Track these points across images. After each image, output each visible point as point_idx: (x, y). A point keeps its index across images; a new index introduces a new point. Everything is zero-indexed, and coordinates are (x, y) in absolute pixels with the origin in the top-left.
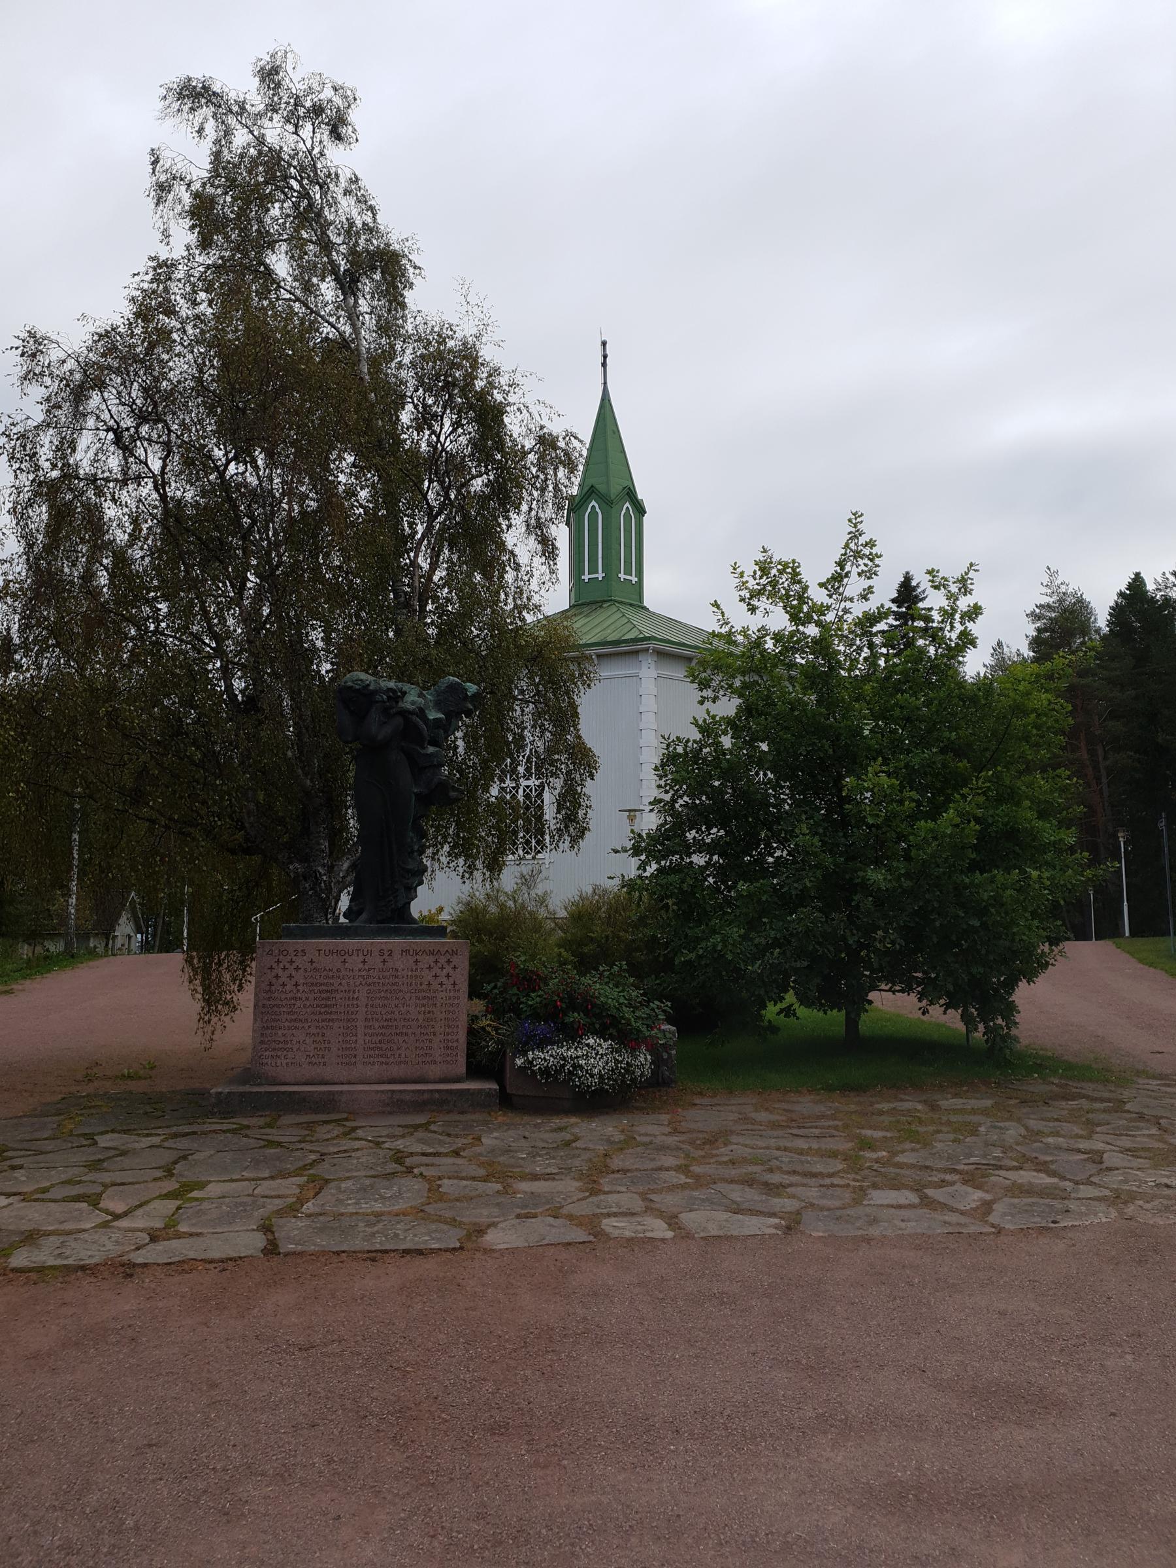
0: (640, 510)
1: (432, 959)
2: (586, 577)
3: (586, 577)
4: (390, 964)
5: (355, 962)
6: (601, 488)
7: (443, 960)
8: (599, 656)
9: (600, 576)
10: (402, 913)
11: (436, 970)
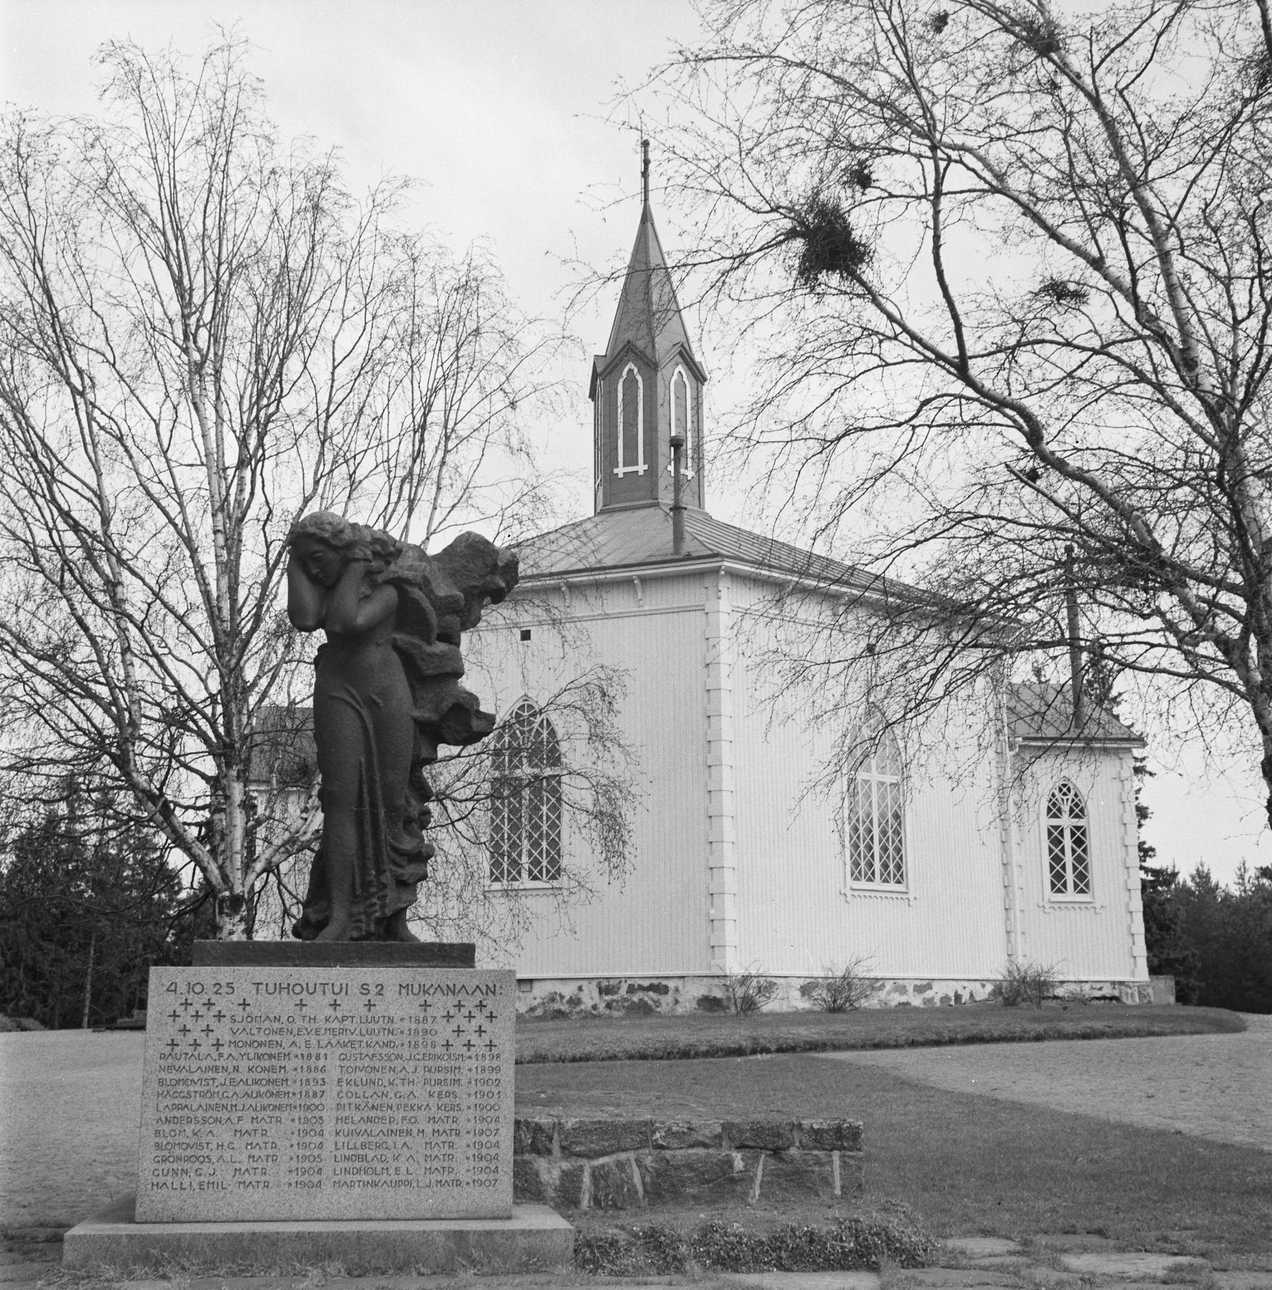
0: (699, 376)
1: (451, 1000)
2: (620, 471)
3: (620, 471)
4: (379, 1010)
5: (319, 1005)
6: (641, 344)
7: (470, 1003)
8: (644, 580)
9: (641, 468)
10: (392, 925)
11: (460, 1020)
